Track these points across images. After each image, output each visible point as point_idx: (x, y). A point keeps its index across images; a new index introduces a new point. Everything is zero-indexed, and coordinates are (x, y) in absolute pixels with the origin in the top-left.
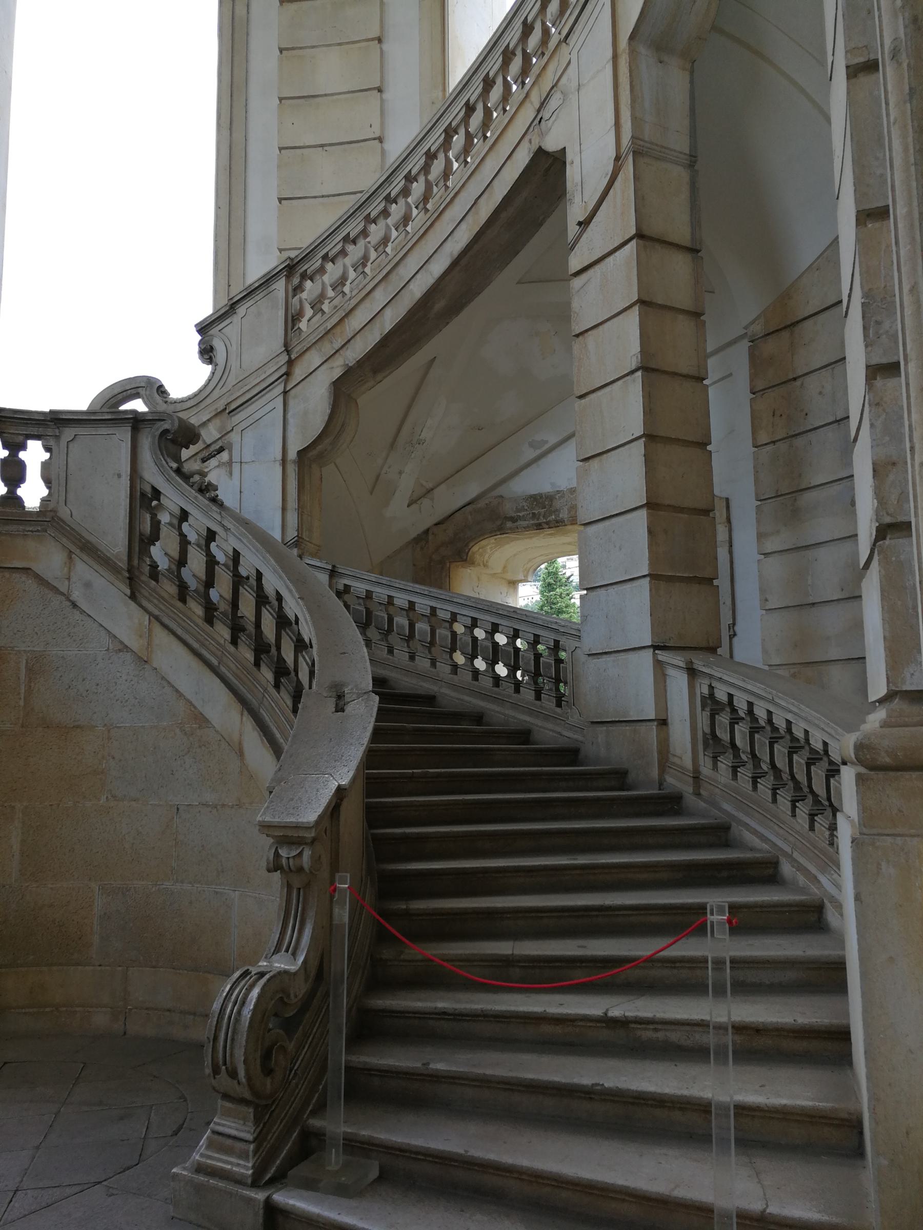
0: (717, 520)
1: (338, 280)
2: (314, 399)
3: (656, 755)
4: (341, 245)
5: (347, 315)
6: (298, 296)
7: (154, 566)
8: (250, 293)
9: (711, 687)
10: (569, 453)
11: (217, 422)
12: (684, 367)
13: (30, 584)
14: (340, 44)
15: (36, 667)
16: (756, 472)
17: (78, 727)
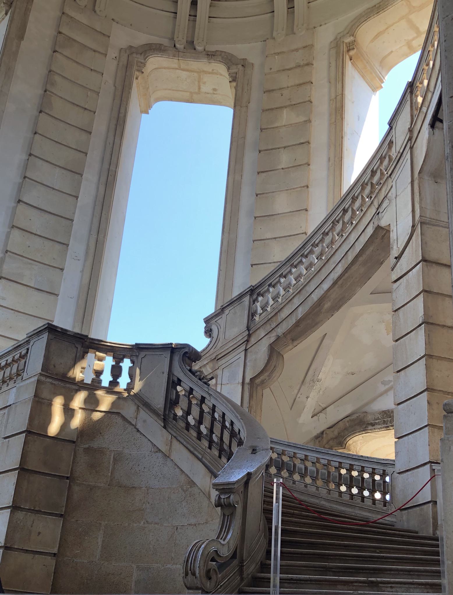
2: (260, 353)
3: (431, 520)
5: (279, 311)
7: (175, 415)
8: (232, 303)
11: (211, 365)
13: (119, 420)
14: (287, 190)
15: (118, 458)
17: (133, 487)
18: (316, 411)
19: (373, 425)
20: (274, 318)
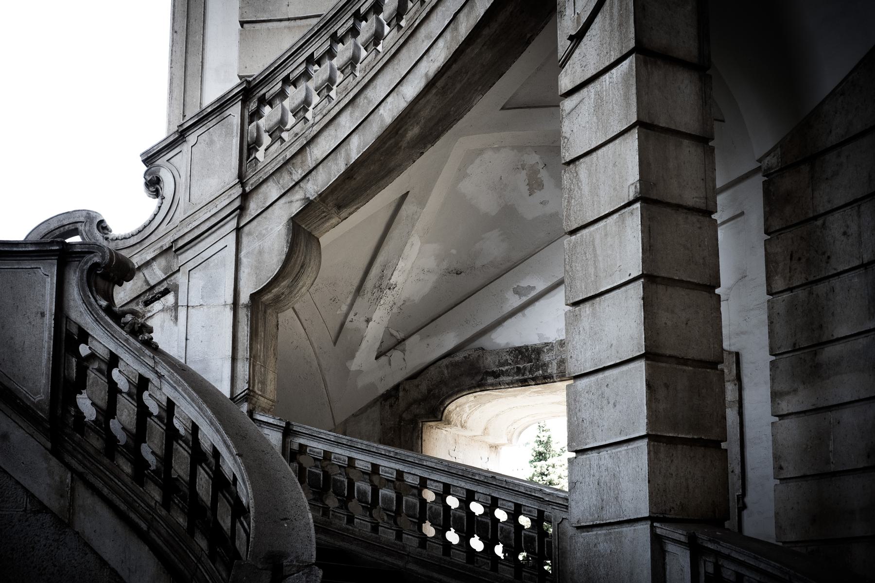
0: (727, 378)
1: (299, 105)
2: (270, 238)
4: (304, 66)
5: (309, 143)
6: (255, 123)
8: (203, 119)
9: (718, 568)
10: (557, 303)
11: (162, 261)
12: (691, 198)
16: (771, 323)
18: (386, 346)
19: (496, 375)
20: (299, 159)
